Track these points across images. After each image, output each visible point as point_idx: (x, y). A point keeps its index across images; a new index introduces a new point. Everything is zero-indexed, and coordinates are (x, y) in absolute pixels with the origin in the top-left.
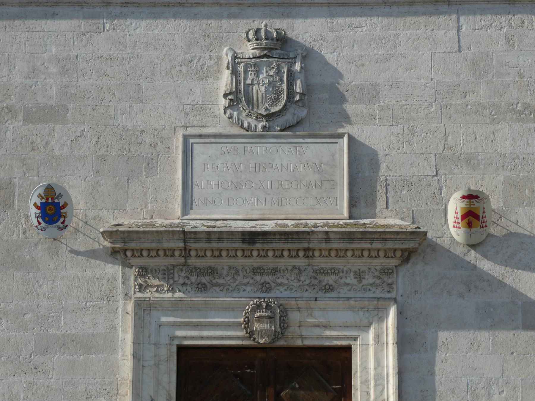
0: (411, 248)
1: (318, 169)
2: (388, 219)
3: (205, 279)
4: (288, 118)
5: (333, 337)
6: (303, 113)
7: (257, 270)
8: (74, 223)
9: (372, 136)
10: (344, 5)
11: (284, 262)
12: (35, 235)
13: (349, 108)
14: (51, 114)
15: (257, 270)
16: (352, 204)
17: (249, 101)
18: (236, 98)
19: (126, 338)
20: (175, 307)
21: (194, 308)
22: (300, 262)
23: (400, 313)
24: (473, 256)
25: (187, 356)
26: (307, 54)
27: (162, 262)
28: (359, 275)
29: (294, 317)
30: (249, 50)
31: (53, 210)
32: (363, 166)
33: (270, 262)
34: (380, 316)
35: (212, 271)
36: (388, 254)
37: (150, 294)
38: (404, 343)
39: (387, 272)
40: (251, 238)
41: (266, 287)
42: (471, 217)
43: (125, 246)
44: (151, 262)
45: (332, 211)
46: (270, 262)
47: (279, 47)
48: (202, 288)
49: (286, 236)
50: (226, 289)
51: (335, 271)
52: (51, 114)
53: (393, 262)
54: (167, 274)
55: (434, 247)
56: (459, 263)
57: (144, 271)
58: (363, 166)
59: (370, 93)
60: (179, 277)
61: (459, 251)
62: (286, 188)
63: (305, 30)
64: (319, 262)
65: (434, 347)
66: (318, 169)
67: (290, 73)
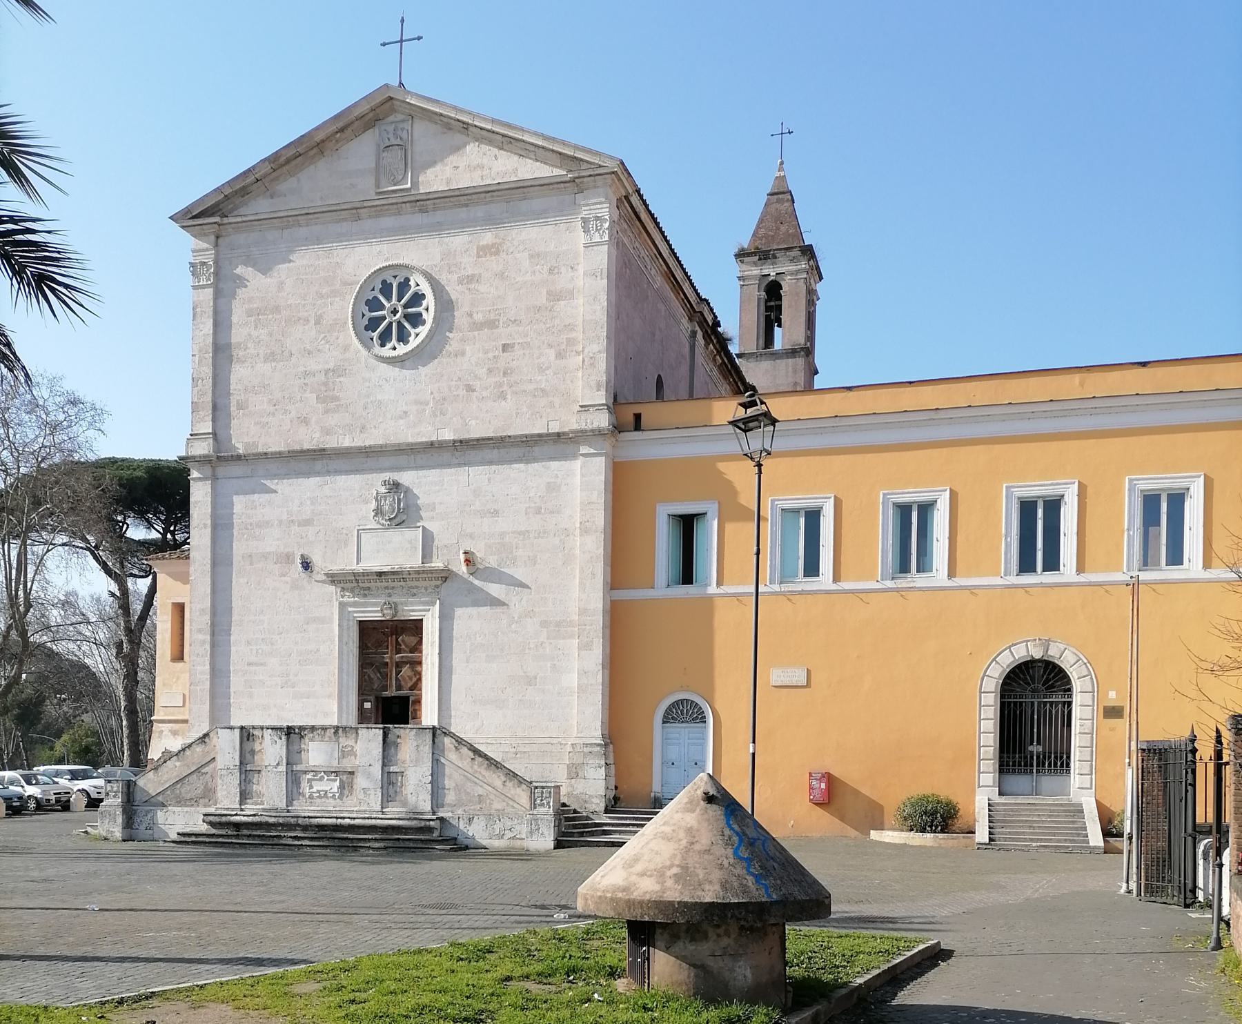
0: (446, 576)
1: (410, 542)
2: (437, 564)
3: (366, 592)
4: (398, 520)
5: (414, 616)
6: (404, 517)
7: (386, 588)
8: (316, 569)
9: (432, 526)
10: (677, 286)
11: (396, 584)
12: (303, 575)
13: (422, 513)
14: (307, 523)
15: (386, 588)
16: (424, 557)
17: (382, 513)
18: (378, 512)
19: (336, 617)
20: (354, 604)
21: (363, 605)
22: (402, 583)
23: (441, 604)
24: (471, 578)
25: (365, 628)
26: (407, 491)
27: (349, 585)
28: (426, 589)
29: (400, 607)
30: (383, 490)
31: (306, 565)
32: (428, 538)
33: (391, 584)
34: (433, 604)
35: (369, 588)
36: (436, 579)
37: (345, 599)
38: (442, 617)
39: (437, 587)
40: (380, 574)
41: (390, 595)
42: (467, 561)
43: (333, 578)
44: (346, 586)
45: (413, 561)
46: (391, 584)
47: (395, 487)
48: (365, 596)
49: (393, 573)
50: (375, 597)
51: (417, 587)
52: (307, 523)
53: (439, 582)
54: (352, 590)
55: (456, 575)
56: (466, 581)
57: (343, 589)
58: (428, 538)
59: (432, 507)
60: (356, 591)
61: (466, 576)
62: (394, 551)
63: (406, 478)
64: (410, 583)
65: (453, 619)
66: (410, 542)
67: (399, 500)
